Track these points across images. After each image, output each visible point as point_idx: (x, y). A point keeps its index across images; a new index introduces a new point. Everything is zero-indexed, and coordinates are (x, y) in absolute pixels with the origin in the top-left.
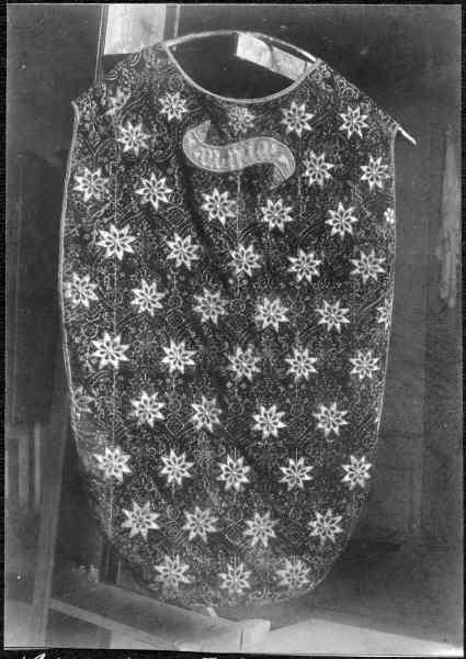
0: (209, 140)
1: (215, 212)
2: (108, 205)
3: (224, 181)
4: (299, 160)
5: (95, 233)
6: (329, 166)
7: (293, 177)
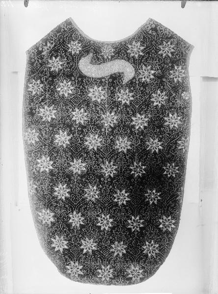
2: (43, 97)
3: (100, 82)
4: (136, 70)
5: (37, 110)
6: (153, 72)
7: (134, 78)
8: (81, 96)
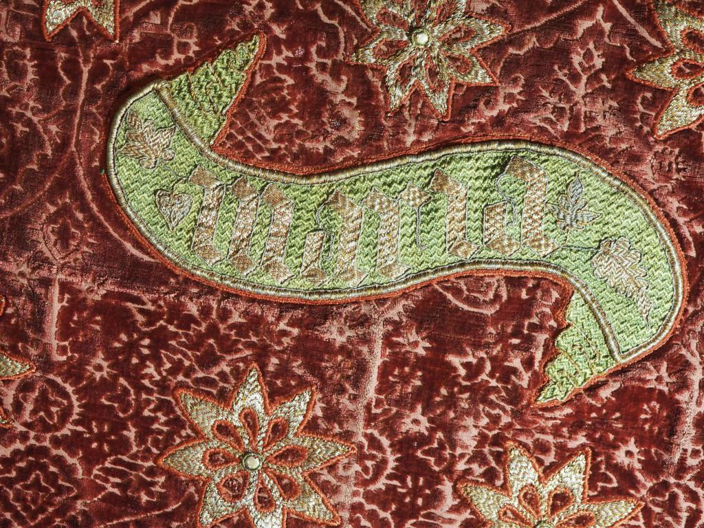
0: (238, 143)
1: (235, 490)
8: (91, 459)
